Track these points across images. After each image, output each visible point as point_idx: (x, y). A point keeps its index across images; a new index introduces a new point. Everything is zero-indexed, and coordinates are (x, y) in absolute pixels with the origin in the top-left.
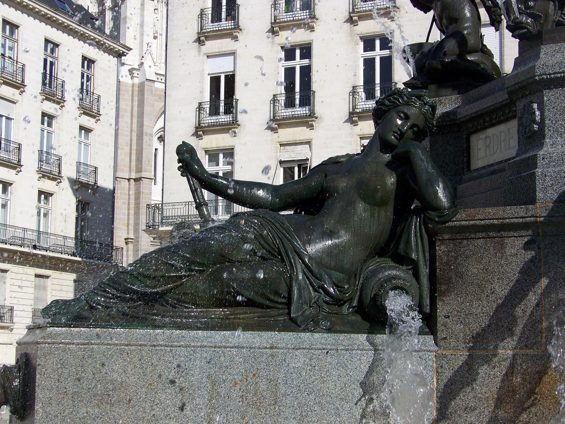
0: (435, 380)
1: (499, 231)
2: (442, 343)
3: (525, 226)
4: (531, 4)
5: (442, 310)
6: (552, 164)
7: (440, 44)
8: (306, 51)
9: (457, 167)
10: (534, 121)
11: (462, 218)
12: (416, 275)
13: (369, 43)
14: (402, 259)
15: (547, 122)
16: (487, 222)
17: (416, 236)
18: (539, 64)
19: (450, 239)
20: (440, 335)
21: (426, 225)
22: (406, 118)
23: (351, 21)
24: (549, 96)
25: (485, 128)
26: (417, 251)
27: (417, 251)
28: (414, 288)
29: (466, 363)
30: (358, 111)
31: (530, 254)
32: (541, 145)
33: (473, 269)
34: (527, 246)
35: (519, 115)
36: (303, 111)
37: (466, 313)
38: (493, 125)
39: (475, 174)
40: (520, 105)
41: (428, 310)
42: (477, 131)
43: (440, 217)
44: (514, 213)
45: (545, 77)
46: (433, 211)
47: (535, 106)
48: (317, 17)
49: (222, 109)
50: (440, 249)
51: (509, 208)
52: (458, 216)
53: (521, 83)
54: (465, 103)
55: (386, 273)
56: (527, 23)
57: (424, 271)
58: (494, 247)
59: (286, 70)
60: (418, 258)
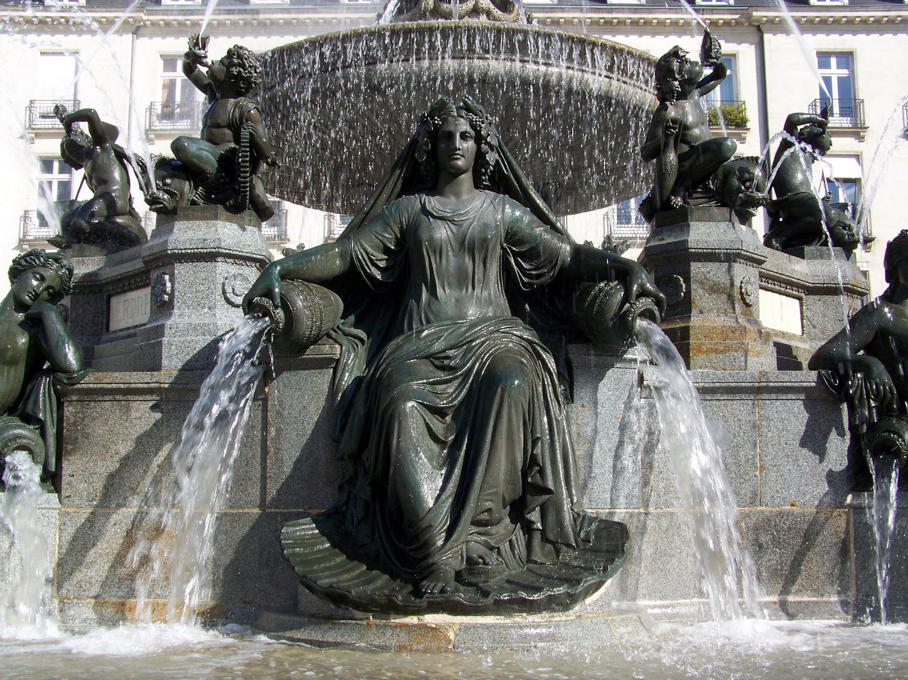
0: (57, 537)
1: (125, 395)
2: (66, 501)
3: (150, 391)
4: (168, 181)
5: (67, 468)
6: (178, 334)
7: (90, 204)
9: (93, 329)
10: (165, 292)
11: (90, 381)
12: (43, 434)
14: (29, 419)
15: (176, 294)
16: (114, 386)
17: (44, 396)
18: (172, 238)
19: (77, 401)
20: (64, 493)
21: (54, 386)
22: (43, 279)
24: (180, 269)
25: (124, 292)
26: (45, 411)
27: (45, 411)
28: (39, 450)
29: (88, 520)
30: (29, 238)
31: (158, 415)
32: (170, 315)
33: (99, 430)
34: (154, 408)
35: (152, 284)
37: (85, 473)
38: (131, 290)
39: (113, 336)
40: (154, 275)
41: (53, 468)
42: (118, 294)
43: (68, 379)
44: (140, 379)
45: (176, 251)
46: (62, 372)
47: (167, 277)
50: (69, 410)
51: (135, 373)
52: (87, 379)
53: (155, 254)
54: (107, 264)
55: (11, 433)
56: (164, 199)
57: (51, 431)
58: (120, 410)
60: (45, 417)
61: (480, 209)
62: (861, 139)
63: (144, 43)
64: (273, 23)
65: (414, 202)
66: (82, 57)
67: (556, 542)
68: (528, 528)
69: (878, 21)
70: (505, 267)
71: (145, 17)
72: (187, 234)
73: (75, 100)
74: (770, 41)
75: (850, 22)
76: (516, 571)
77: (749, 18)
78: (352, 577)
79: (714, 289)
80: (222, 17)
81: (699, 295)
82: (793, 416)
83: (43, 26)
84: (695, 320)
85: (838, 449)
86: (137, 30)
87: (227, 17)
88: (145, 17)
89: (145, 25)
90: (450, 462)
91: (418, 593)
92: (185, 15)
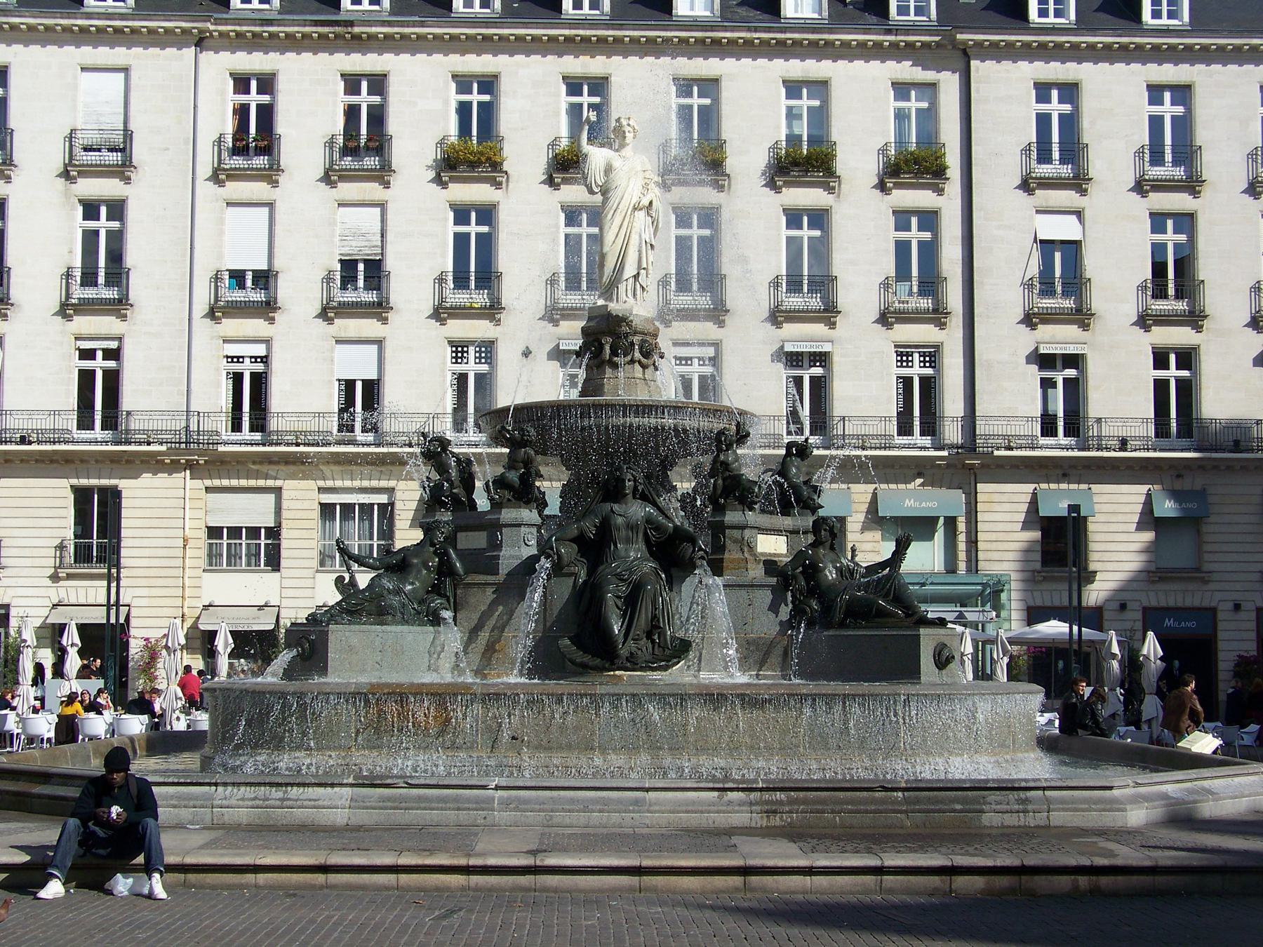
8: (117, 209)
11: (469, 580)
13: (90, 209)
23: (65, 175)
33: (472, 600)
36: (111, 294)
44: (491, 579)
48: (15, 162)
49: (1171, 291)
50: (459, 592)
59: (456, 235)
61: (637, 510)
62: (1083, 192)
63: (207, 57)
64: (371, 37)
65: (607, 506)
66: (134, 75)
67: (663, 647)
68: (653, 642)
69: (1108, 47)
70: (646, 534)
71: (212, 28)
72: (507, 515)
73: (126, 129)
74: (977, 70)
75: (1075, 47)
76: (648, 657)
77: (954, 42)
78: (580, 657)
79: (735, 541)
80: (307, 29)
81: (728, 542)
82: (766, 597)
83: (82, 37)
84: (727, 555)
85: (785, 612)
86: (201, 42)
87: (314, 29)
88: (212, 28)
89: (211, 35)
90: (624, 616)
91: (613, 664)
92: (262, 25)
